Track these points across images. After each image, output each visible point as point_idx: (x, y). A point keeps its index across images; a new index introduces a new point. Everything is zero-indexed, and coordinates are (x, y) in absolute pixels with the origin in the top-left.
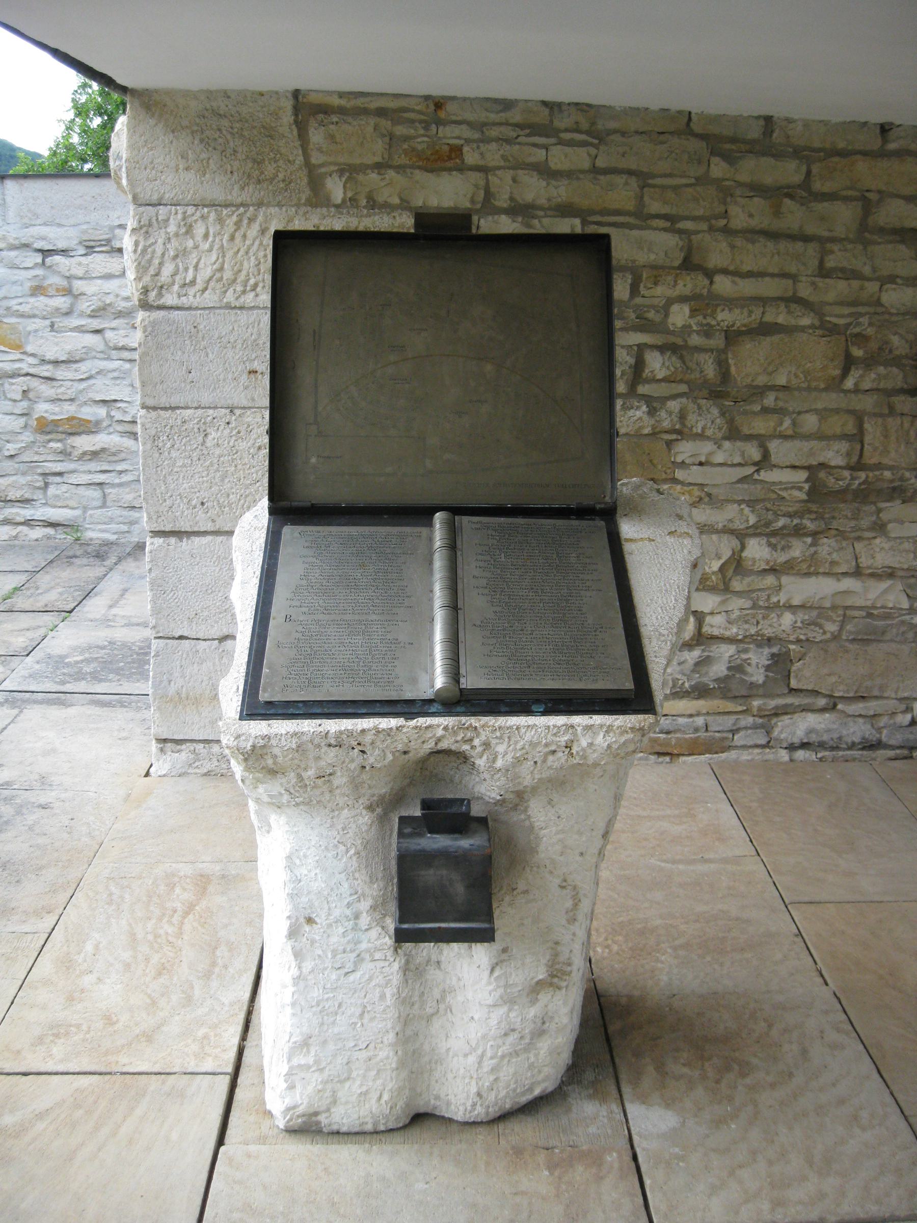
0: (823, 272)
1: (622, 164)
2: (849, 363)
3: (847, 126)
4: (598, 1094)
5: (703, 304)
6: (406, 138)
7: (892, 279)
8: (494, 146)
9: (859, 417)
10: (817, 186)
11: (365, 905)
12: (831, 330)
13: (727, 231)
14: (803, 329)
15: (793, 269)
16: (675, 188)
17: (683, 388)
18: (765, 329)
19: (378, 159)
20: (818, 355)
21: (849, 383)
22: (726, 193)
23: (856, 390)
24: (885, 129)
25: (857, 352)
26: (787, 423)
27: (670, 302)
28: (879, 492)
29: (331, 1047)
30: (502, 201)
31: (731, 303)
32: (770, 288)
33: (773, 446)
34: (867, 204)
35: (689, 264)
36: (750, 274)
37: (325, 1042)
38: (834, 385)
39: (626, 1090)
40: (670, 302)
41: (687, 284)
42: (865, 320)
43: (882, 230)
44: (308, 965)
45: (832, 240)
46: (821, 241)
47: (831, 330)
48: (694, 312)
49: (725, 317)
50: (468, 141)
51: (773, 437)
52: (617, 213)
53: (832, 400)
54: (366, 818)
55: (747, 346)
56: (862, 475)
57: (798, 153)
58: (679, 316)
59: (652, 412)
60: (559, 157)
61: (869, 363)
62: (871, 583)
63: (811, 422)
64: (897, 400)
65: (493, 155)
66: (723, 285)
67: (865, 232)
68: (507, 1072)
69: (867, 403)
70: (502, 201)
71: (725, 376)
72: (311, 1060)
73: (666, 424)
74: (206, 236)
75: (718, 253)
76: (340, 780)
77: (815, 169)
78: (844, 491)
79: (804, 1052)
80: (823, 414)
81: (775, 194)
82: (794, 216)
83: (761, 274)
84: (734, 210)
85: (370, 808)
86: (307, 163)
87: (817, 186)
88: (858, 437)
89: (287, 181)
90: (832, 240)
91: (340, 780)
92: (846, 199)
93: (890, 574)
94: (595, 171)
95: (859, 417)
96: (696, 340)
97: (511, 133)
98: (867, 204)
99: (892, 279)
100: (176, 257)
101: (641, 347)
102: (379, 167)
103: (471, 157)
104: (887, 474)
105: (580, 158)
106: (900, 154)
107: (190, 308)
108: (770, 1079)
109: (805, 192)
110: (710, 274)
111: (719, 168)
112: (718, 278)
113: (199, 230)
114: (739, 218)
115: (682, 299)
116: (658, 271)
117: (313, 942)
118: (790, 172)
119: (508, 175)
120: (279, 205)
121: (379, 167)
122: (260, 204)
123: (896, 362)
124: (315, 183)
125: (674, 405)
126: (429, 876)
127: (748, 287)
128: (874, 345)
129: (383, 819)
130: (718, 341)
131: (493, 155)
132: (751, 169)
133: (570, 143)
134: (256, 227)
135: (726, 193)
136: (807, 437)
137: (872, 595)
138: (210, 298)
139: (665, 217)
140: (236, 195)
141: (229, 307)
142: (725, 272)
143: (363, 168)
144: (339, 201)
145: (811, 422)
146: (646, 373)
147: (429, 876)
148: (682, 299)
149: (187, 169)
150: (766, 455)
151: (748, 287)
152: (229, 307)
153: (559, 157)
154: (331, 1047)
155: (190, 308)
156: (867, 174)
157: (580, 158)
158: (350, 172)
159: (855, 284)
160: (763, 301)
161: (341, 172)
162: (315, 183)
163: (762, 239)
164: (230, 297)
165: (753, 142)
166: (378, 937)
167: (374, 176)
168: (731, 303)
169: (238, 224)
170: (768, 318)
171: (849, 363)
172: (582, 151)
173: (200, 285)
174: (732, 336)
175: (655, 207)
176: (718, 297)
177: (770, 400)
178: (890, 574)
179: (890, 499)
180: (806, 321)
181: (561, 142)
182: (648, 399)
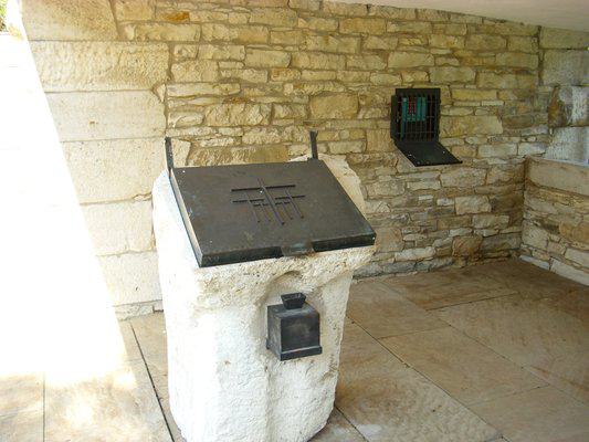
0: (347, 68)
1: (261, 21)
2: (359, 107)
3: (353, 6)
4: (342, 425)
5: (298, 84)
6: (161, 9)
7: (374, 71)
8: (204, 13)
9: (365, 130)
10: (342, 31)
11: (253, 350)
12: (352, 94)
13: (306, 51)
14: (340, 93)
15: (334, 67)
16: (284, 32)
17: (292, 121)
18: (323, 94)
19: (150, 18)
20: (347, 104)
21: (360, 116)
22: (304, 34)
23: (363, 119)
24: (368, 7)
25: (363, 103)
26: (337, 135)
27: (285, 83)
28: (374, 163)
29: (237, 423)
30: (209, 38)
31: (309, 83)
32: (326, 75)
33: (331, 145)
34: (362, 39)
35: (291, 66)
36: (318, 70)
37: (235, 420)
38: (354, 117)
39: (353, 421)
40: (285, 83)
41: (291, 75)
42: (365, 89)
43: (369, 50)
44: (226, 384)
45: (350, 54)
46: (345, 54)
47: (352, 94)
48: (295, 87)
49: (308, 89)
50: (192, 10)
51: (330, 141)
52: (259, 43)
53: (354, 124)
54: (254, 308)
55: (318, 101)
56: (368, 156)
57: (336, 17)
58: (289, 89)
59: (280, 133)
60: (234, 18)
61: (368, 107)
62: (374, 202)
63: (346, 134)
64: (380, 122)
65: (204, 16)
66: (307, 75)
67: (361, 50)
68: (311, 421)
69: (367, 124)
70: (209, 38)
71: (309, 115)
72: (228, 430)
73: (286, 138)
74: (66, 56)
75: (303, 61)
76: (246, 291)
77: (341, 24)
78: (360, 164)
79: (415, 393)
80: (351, 130)
81: (326, 35)
82: (334, 43)
83: (322, 70)
84: (309, 42)
85: (256, 304)
86: (116, 20)
87: (342, 31)
88: (365, 139)
89: (106, 29)
90: (350, 54)
91: (246, 291)
92: (354, 37)
93: (381, 198)
94: (249, 24)
95: (365, 131)
96: (296, 99)
97: (211, 6)
98: (362, 39)
99: (374, 71)
100: (50, 67)
101: (273, 103)
102: (150, 22)
103: (193, 17)
104: (378, 155)
105: (243, 18)
106: (374, 17)
107: (59, 93)
108: (408, 404)
109: (337, 34)
110: (300, 70)
111: (301, 23)
112: (304, 72)
113: (62, 53)
114: (311, 45)
115: (289, 82)
116: (279, 69)
117: (228, 373)
118: (331, 24)
119: (211, 26)
120: (102, 40)
121: (150, 22)
122: (93, 40)
123: (378, 106)
124: (120, 30)
125: (289, 129)
126: (294, 327)
127: (316, 75)
128: (369, 100)
129: (260, 308)
130: (306, 100)
131: (204, 16)
132: (315, 23)
133: (238, 12)
134: (92, 51)
135: (304, 34)
136: (344, 140)
137: (375, 208)
138: (70, 87)
139: (280, 45)
140: (80, 36)
141: (79, 91)
142: (307, 69)
143: (143, 23)
144: (132, 38)
145: (346, 134)
146: (276, 115)
147: (294, 327)
148: (289, 82)
149: (55, 23)
150: (328, 149)
151: (316, 75)
152: (79, 91)
153: (234, 18)
154: (237, 423)
155: (59, 93)
156: (362, 26)
157: (243, 18)
158: (137, 24)
159: (361, 73)
160: (323, 81)
161: (132, 25)
162: (120, 30)
163: (322, 55)
164: (79, 86)
165: (315, 12)
166: (257, 365)
167: (148, 26)
168: (309, 83)
169: (82, 50)
170: (326, 89)
171: (359, 107)
172: (244, 16)
173: (63, 80)
174: (311, 97)
175: (276, 40)
176: (304, 80)
177: (329, 125)
178: (381, 198)
179: (379, 165)
180: (341, 90)
181: (234, 11)
182: (278, 127)
